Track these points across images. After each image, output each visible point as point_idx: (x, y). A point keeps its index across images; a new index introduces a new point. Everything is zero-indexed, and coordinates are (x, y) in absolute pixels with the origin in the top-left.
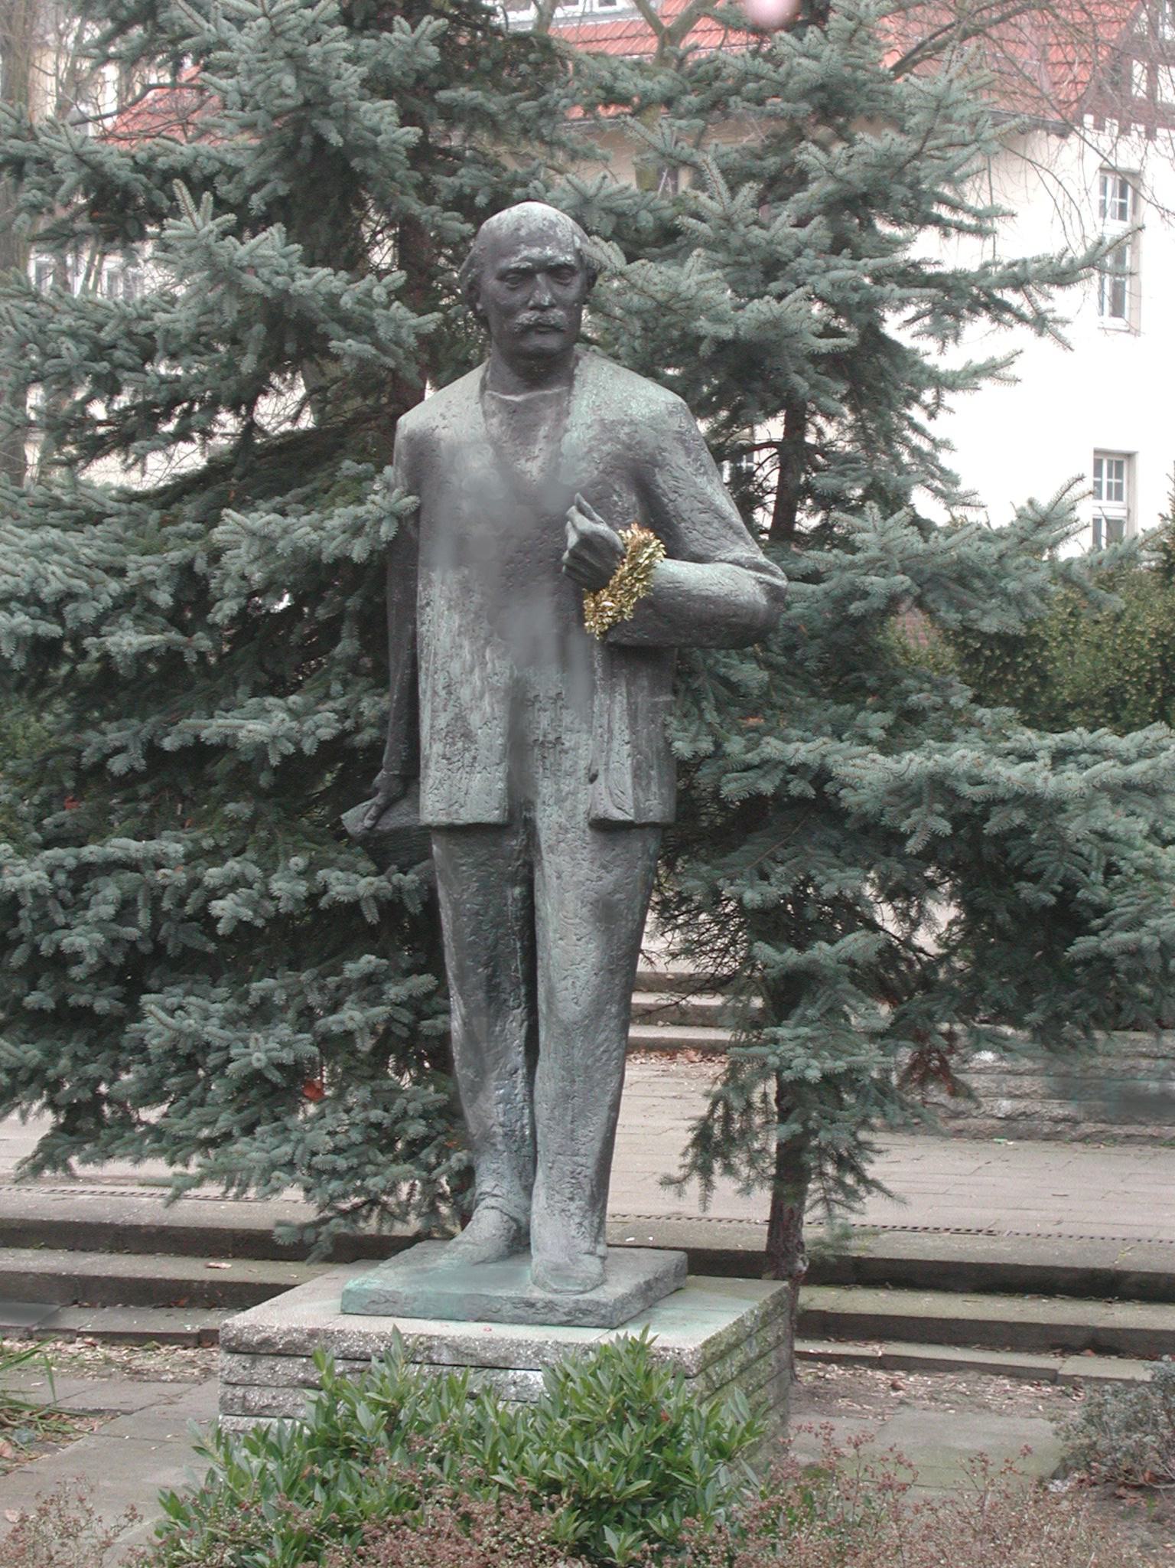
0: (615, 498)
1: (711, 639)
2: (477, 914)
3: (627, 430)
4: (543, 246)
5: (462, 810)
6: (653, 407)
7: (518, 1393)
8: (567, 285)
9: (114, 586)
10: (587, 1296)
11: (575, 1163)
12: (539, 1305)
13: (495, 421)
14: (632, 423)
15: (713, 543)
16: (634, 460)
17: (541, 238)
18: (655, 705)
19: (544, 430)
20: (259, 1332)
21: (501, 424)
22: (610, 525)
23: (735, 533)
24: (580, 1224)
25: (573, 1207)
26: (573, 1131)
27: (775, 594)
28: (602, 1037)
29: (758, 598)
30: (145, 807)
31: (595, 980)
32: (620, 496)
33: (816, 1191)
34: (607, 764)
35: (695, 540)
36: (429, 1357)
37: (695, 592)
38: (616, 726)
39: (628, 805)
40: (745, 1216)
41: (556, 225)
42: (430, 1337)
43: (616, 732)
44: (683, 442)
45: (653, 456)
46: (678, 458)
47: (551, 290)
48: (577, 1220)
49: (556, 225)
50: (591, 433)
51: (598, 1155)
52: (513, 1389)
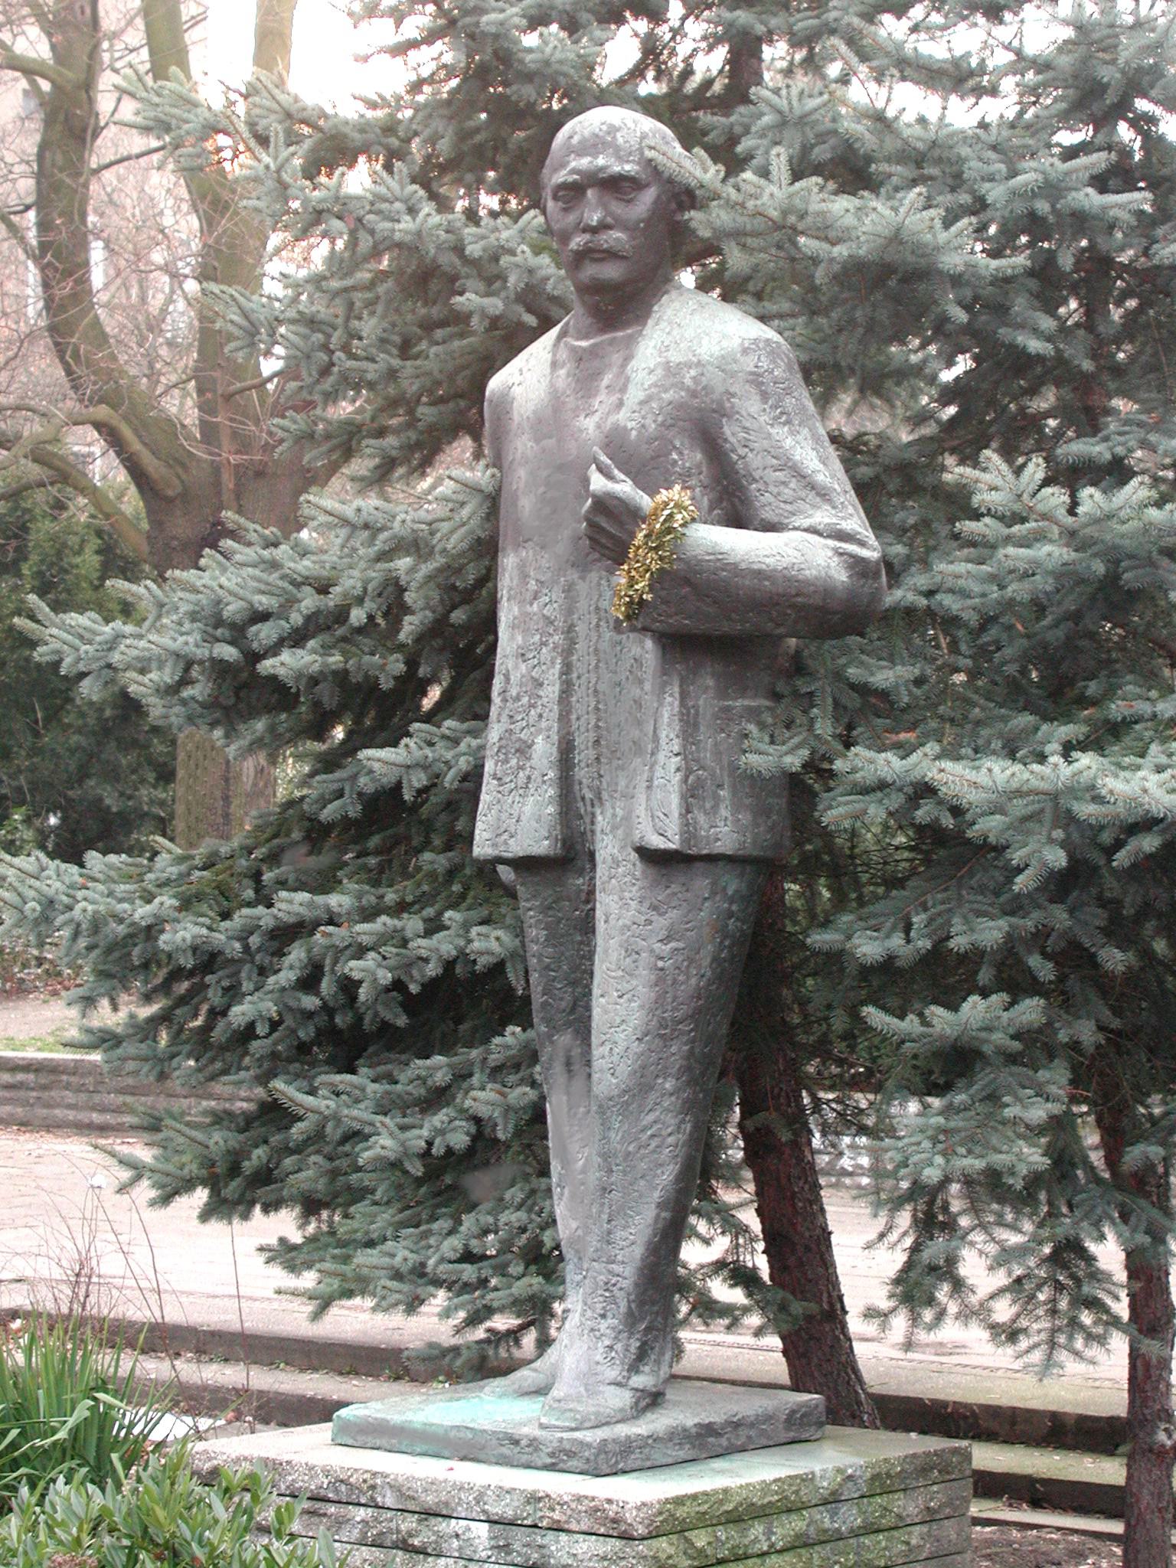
0: (675, 456)
1: (778, 625)
2: (547, 968)
3: (693, 373)
4: (595, 156)
5: (512, 842)
6: (725, 344)
7: (460, 1548)
8: (629, 201)
9: (309, 601)
10: (578, 1435)
11: (610, 1272)
12: (524, 1443)
13: (562, 372)
14: (699, 364)
15: (788, 507)
16: (700, 410)
17: (595, 145)
18: (727, 709)
19: (607, 379)
20: (210, 1459)
21: (568, 375)
22: (638, 484)
23: (818, 494)
24: (611, 1348)
25: (603, 1325)
26: (609, 1233)
27: (859, 567)
28: (651, 1117)
29: (833, 573)
30: (372, 861)
31: (636, 1047)
32: (681, 453)
33: (1039, 1331)
34: (650, 780)
35: (767, 505)
36: (372, 1498)
37: (743, 566)
38: (663, 735)
39: (673, 827)
40: (567, 1325)
41: (618, 129)
42: (374, 1474)
43: (663, 741)
44: (759, 385)
45: (720, 403)
46: (751, 405)
47: (605, 207)
48: (607, 1342)
49: (618, 129)
50: (653, 378)
51: (638, 1263)
52: (455, 1544)
